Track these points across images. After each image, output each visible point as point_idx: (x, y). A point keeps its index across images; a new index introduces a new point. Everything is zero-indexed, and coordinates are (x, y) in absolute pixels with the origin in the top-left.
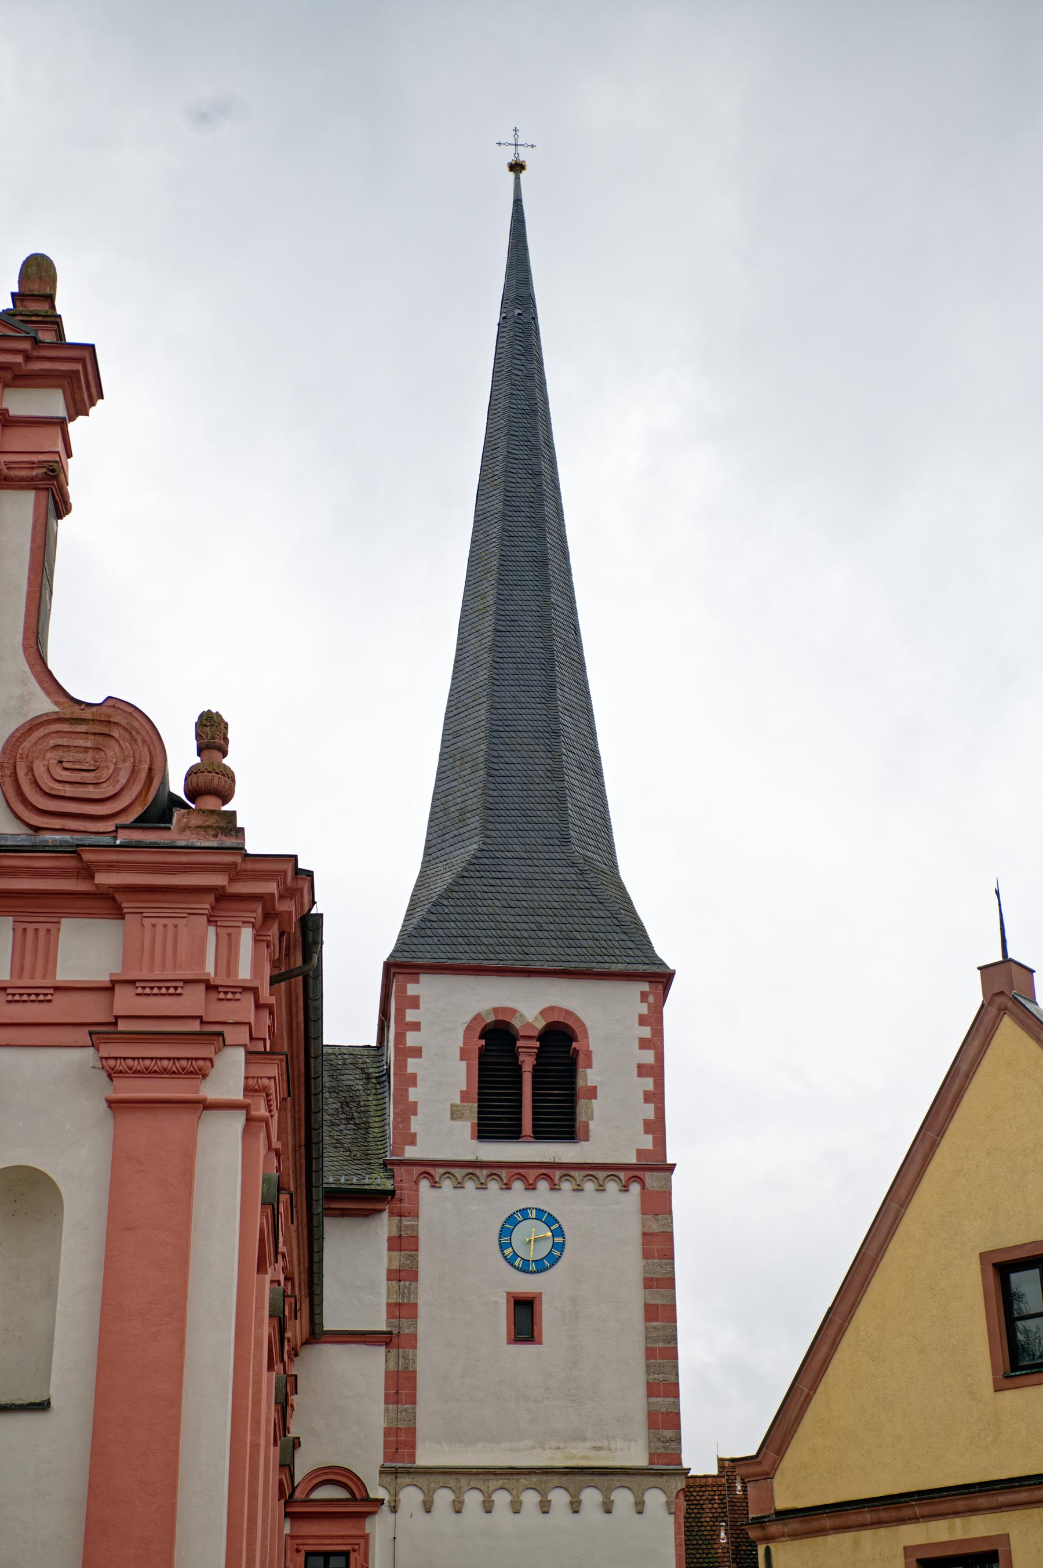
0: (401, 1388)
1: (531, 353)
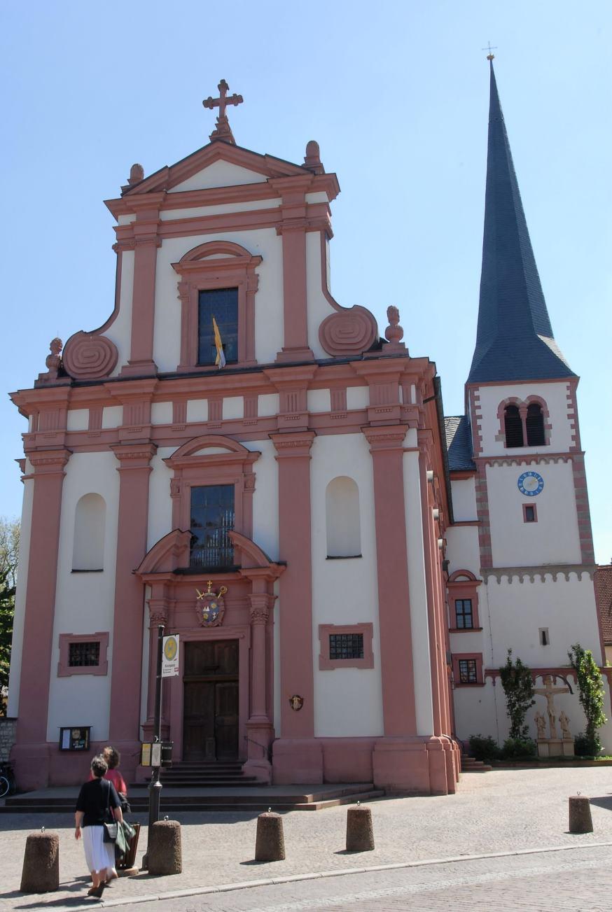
0: (485, 541)
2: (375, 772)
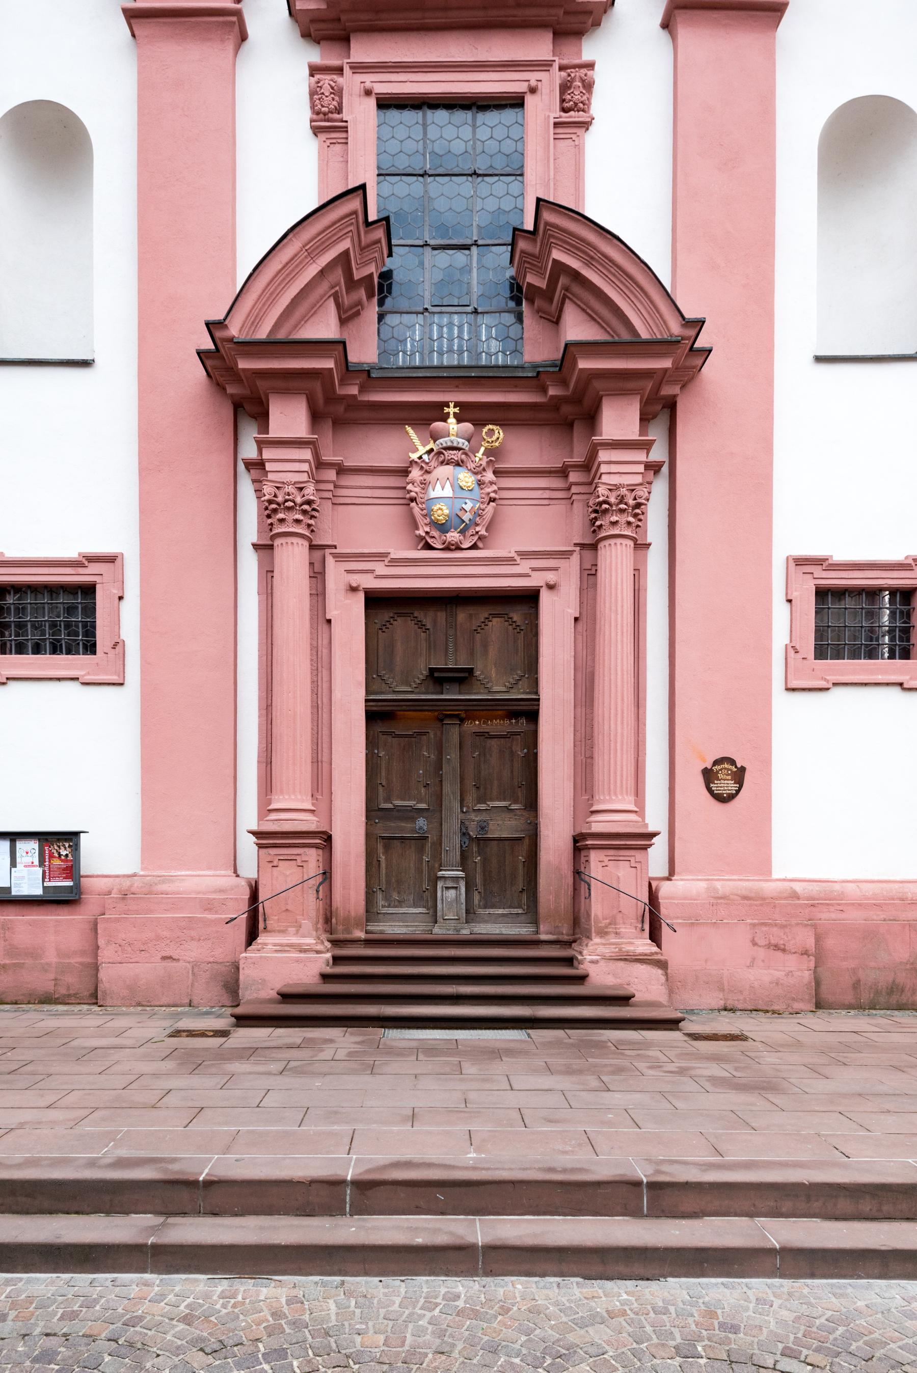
2: (101, 975)
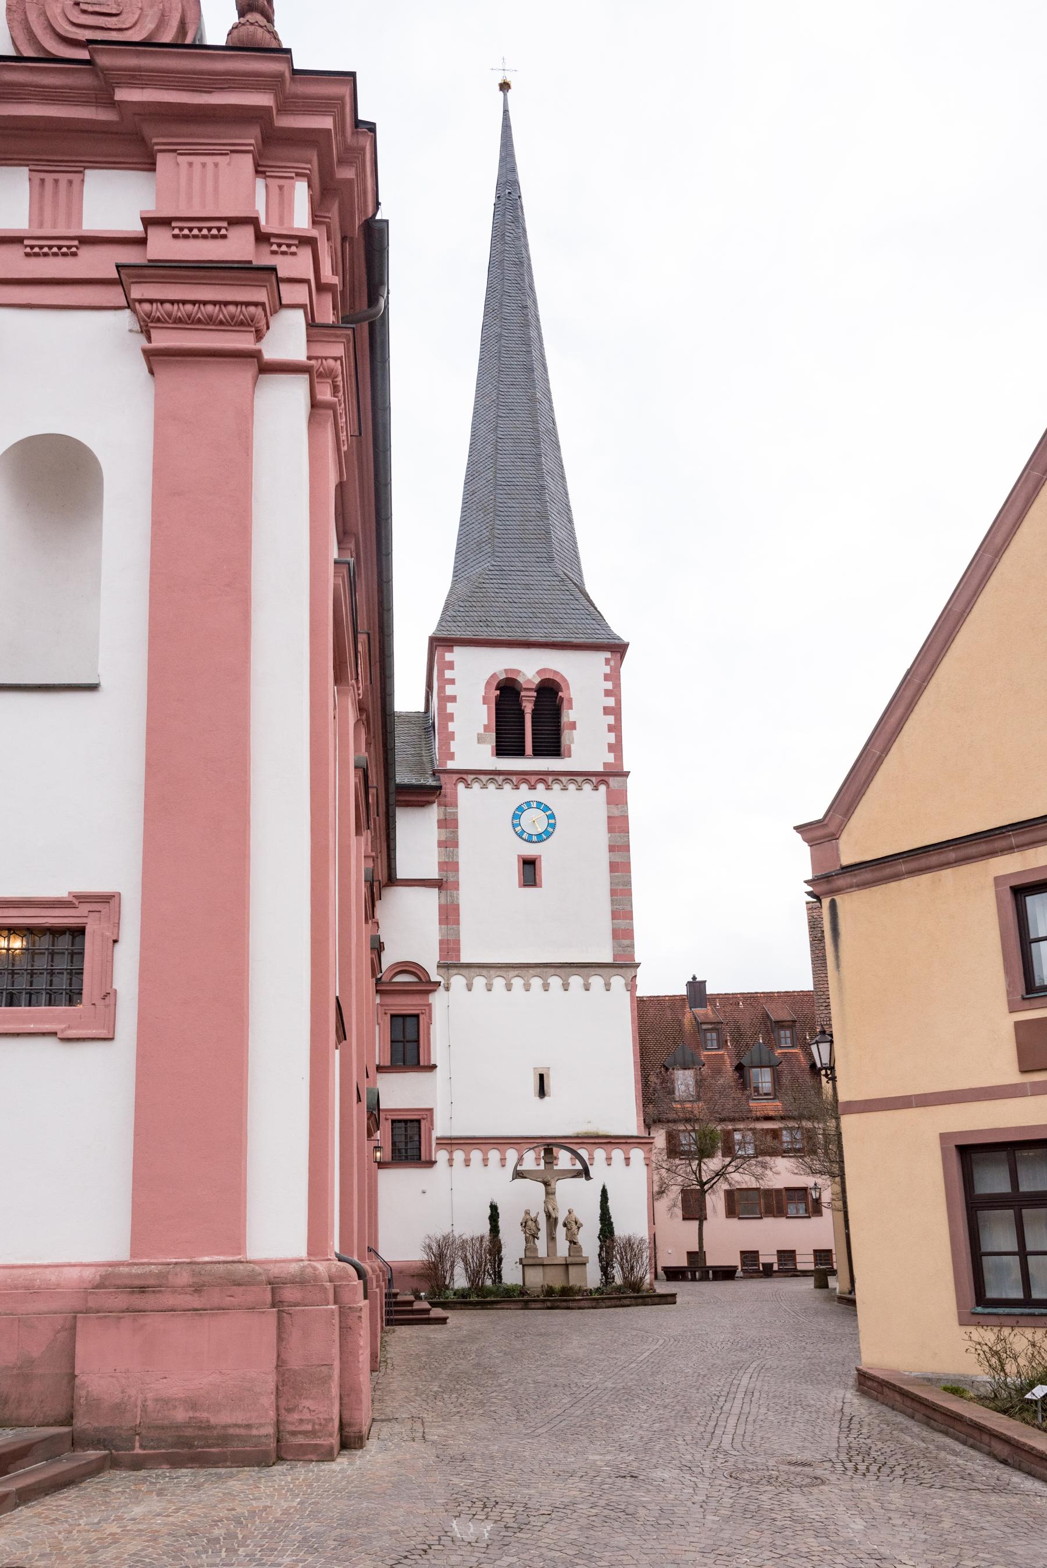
0: (449, 915)
1: (518, 221)
